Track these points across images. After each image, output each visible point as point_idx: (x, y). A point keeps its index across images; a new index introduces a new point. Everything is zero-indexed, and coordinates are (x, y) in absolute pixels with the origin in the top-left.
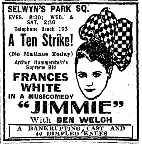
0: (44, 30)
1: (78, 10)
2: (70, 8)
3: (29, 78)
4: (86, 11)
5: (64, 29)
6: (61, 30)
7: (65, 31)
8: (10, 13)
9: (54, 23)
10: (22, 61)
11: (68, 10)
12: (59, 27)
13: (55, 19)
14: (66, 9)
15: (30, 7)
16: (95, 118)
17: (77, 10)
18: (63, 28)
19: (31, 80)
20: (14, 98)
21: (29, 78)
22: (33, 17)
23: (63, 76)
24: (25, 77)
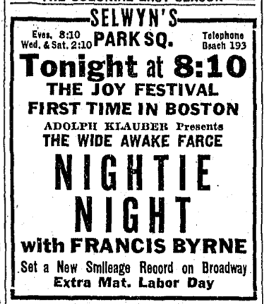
0: (206, 48)
1: (149, 42)
2: (138, 38)
3: (99, 248)
4: (167, 44)
5: (240, 46)
6: (235, 46)
7: (242, 49)
8: (162, 31)
9: (89, 46)
10: (51, 241)
11: (134, 42)
12: (208, 188)
13: (78, 41)
14: (128, 39)
15: (50, 128)
16: (110, 11)
17: (87, 269)
18: (238, 44)
19: (101, 251)
20: (235, 112)
21: (99, 248)
22: (65, 34)
23: (158, 89)
24: (210, 246)
